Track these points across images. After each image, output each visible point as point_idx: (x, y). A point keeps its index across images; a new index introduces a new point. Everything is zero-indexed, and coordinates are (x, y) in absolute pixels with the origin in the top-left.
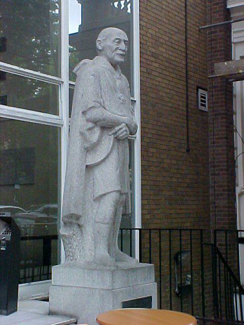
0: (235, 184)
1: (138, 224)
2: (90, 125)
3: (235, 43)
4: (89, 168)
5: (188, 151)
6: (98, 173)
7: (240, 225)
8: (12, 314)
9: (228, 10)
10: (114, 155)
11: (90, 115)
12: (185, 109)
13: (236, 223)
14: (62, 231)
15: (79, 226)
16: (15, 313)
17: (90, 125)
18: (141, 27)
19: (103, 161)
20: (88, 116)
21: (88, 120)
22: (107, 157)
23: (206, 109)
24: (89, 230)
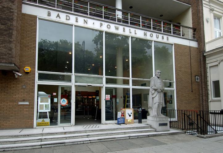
0: (208, 98)
1: (176, 109)
2: (152, 90)
3: (207, 64)
4: (153, 98)
5: (192, 91)
6: (155, 99)
7: (210, 109)
8: (165, 126)
9: (205, 56)
10: (158, 95)
11: (153, 88)
12: (191, 82)
13: (209, 109)
14: (149, 110)
15: (152, 109)
16: (166, 126)
17: (152, 90)
18: (175, 65)
19: (155, 96)
20: (152, 88)
21: (152, 89)
22: (156, 96)
23: (199, 81)
24: (153, 110)
